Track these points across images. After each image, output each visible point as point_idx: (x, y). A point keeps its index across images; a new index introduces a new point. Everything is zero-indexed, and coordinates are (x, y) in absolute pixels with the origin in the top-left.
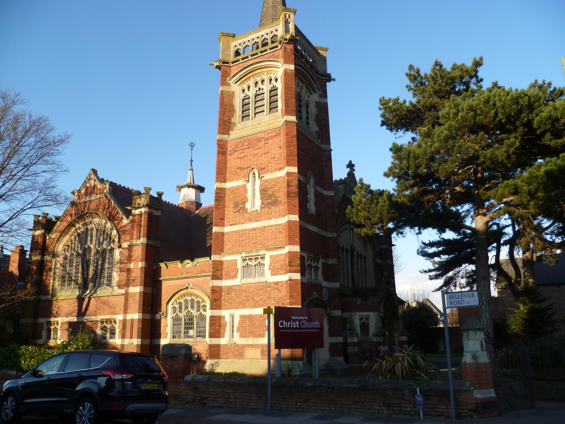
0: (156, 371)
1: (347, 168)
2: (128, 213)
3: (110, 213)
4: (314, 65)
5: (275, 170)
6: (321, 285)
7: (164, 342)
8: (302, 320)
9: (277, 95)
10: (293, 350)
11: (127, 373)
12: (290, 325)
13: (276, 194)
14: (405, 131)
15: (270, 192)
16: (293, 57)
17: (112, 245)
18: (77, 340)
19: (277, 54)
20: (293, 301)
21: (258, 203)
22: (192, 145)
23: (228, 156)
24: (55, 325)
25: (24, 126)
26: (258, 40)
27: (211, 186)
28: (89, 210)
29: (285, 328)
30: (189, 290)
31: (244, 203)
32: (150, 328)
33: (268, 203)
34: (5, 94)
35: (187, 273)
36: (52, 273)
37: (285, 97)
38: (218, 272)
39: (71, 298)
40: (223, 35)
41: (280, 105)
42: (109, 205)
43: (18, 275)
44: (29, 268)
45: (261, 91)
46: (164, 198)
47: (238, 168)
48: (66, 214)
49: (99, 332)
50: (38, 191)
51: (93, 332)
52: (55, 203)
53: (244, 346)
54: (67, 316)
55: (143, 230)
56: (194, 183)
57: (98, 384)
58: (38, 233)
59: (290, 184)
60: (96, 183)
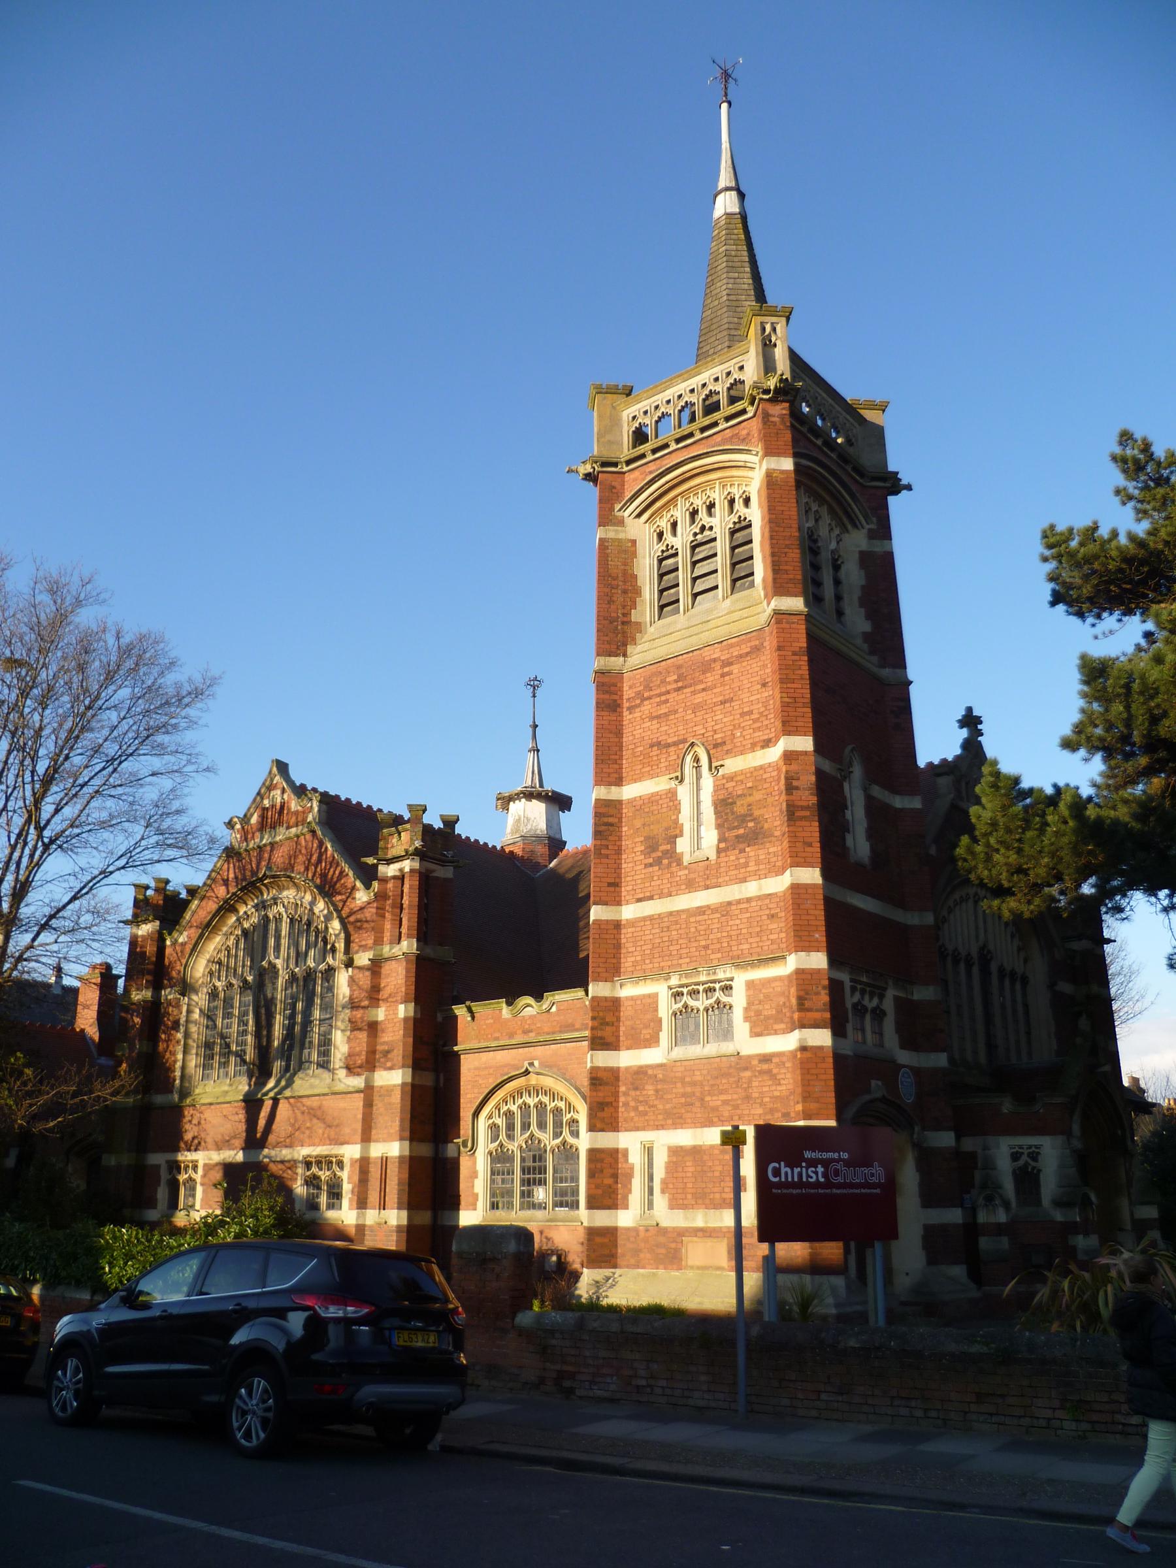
0: (435, 1300)
1: (961, 727)
2: (368, 875)
3: (324, 876)
4: (851, 450)
5: (753, 747)
6: (894, 1062)
7: (468, 1218)
8: (834, 1160)
9: (750, 542)
10: (817, 1245)
11: (359, 1301)
12: (800, 1175)
13: (757, 813)
14: (1124, 614)
15: (740, 808)
16: (788, 436)
17: (330, 960)
18: (241, 1213)
19: (744, 432)
20: (813, 1106)
21: (710, 837)
22: (534, 685)
23: (626, 713)
24: (190, 1171)
25: (105, 660)
26: (693, 399)
27: (587, 796)
28: (269, 868)
29: (787, 1185)
30: (533, 1079)
31: (672, 840)
32: (432, 1181)
33: (737, 837)
34: (56, 582)
35: (526, 1032)
36: (180, 1036)
37: (772, 546)
38: (606, 1028)
39: (228, 1099)
40: (601, 390)
41: (760, 569)
42: (321, 855)
43: (96, 1038)
44: (124, 1021)
45: (707, 533)
46: (461, 829)
47: (652, 746)
48: (214, 880)
49: (299, 1189)
50: (143, 822)
51: (288, 1192)
52: (185, 853)
53: (681, 1233)
54: (218, 1147)
55: (409, 919)
56: (541, 786)
57: (284, 1331)
58: (146, 929)
59: (795, 783)
60: (285, 796)
